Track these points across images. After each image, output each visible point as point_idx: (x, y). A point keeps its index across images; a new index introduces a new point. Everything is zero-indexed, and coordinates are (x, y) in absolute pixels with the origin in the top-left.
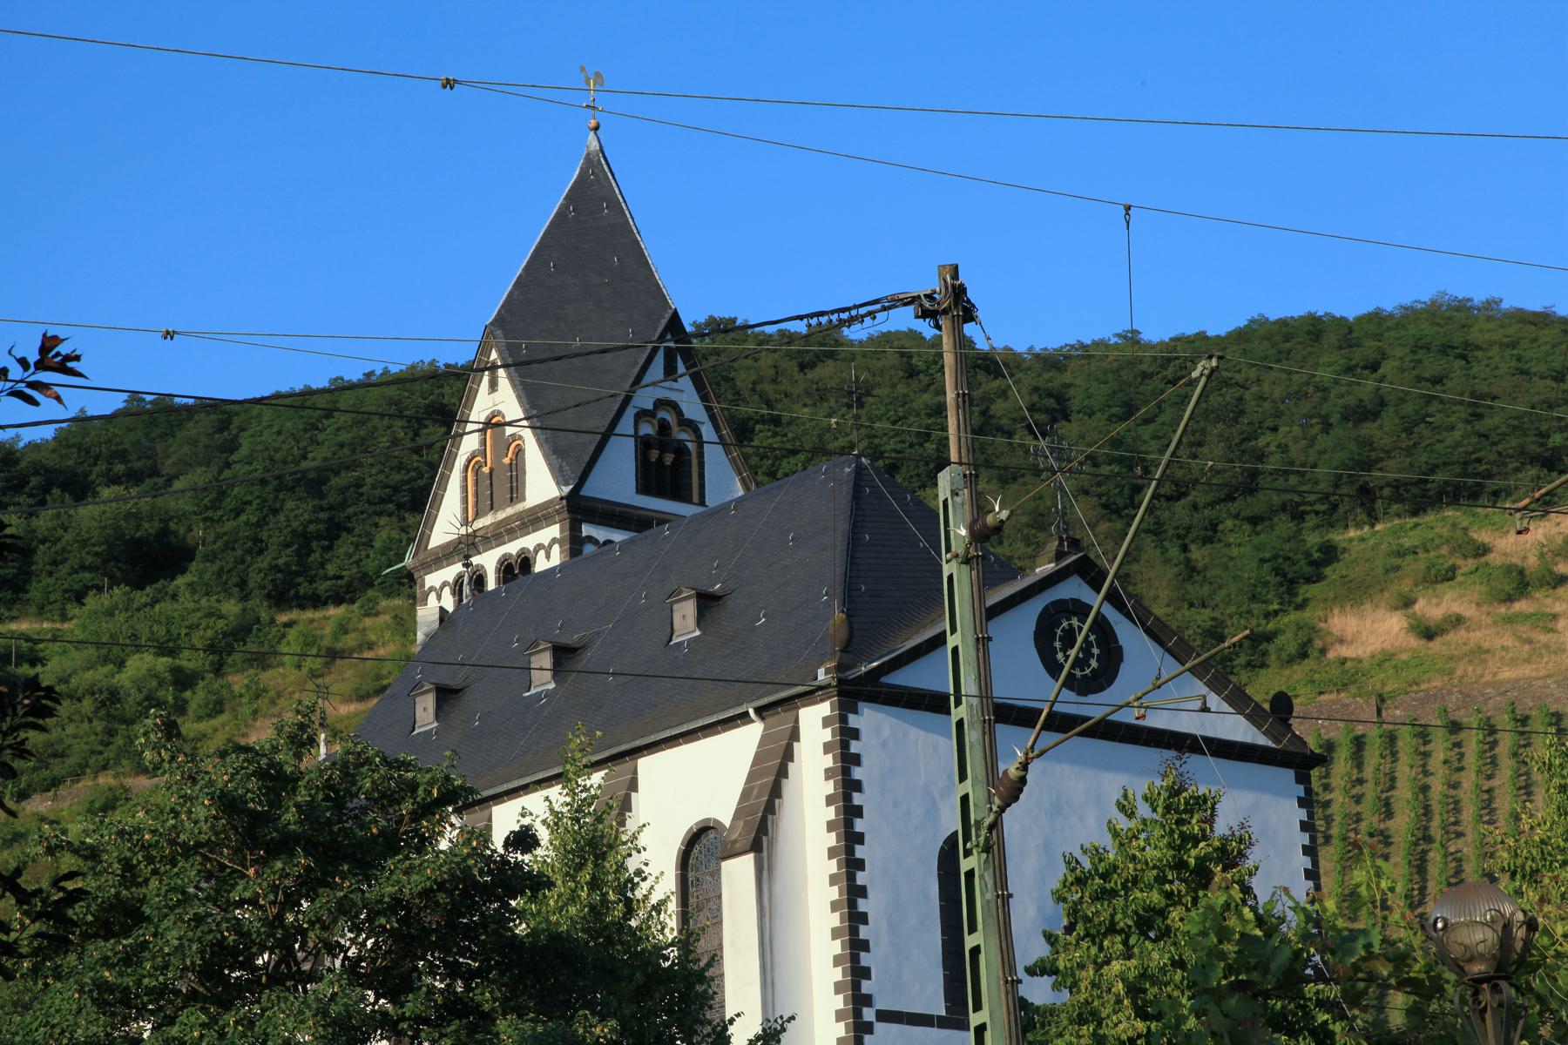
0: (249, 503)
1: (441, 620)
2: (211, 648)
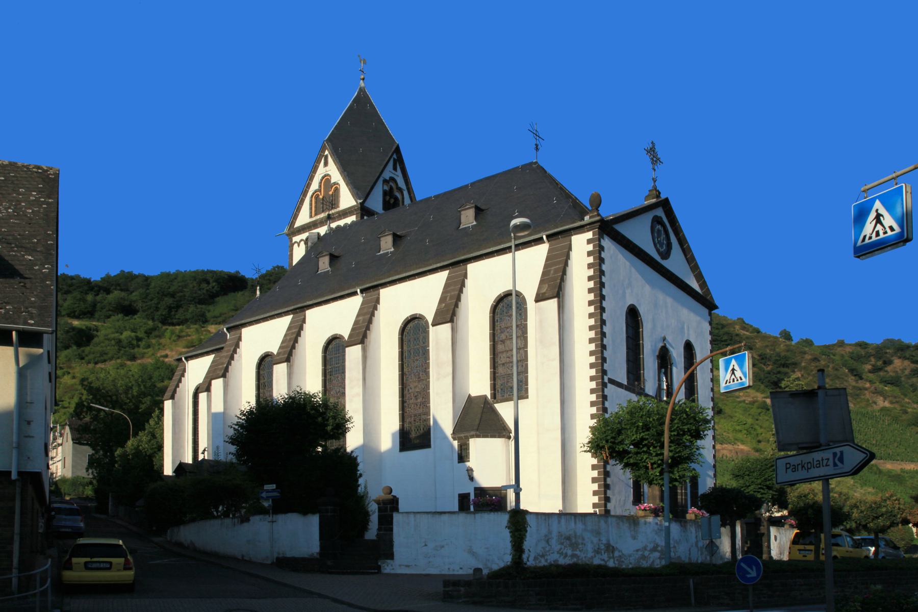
0: (154, 298)
1: (318, 238)
2: (146, 332)
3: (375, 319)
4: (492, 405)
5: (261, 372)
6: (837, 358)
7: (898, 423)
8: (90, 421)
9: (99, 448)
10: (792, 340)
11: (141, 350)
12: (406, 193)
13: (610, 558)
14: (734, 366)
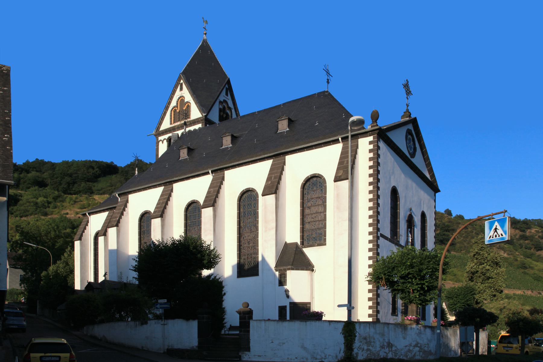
0: (59, 177)
2: (53, 198)
3: (221, 191)
4: (301, 249)
5: (142, 224)
6: (477, 227)
7: (512, 267)
8: (22, 254)
9: (28, 271)
10: (452, 216)
11: (51, 210)
12: (233, 111)
13: (390, 351)
14: (496, 226)
